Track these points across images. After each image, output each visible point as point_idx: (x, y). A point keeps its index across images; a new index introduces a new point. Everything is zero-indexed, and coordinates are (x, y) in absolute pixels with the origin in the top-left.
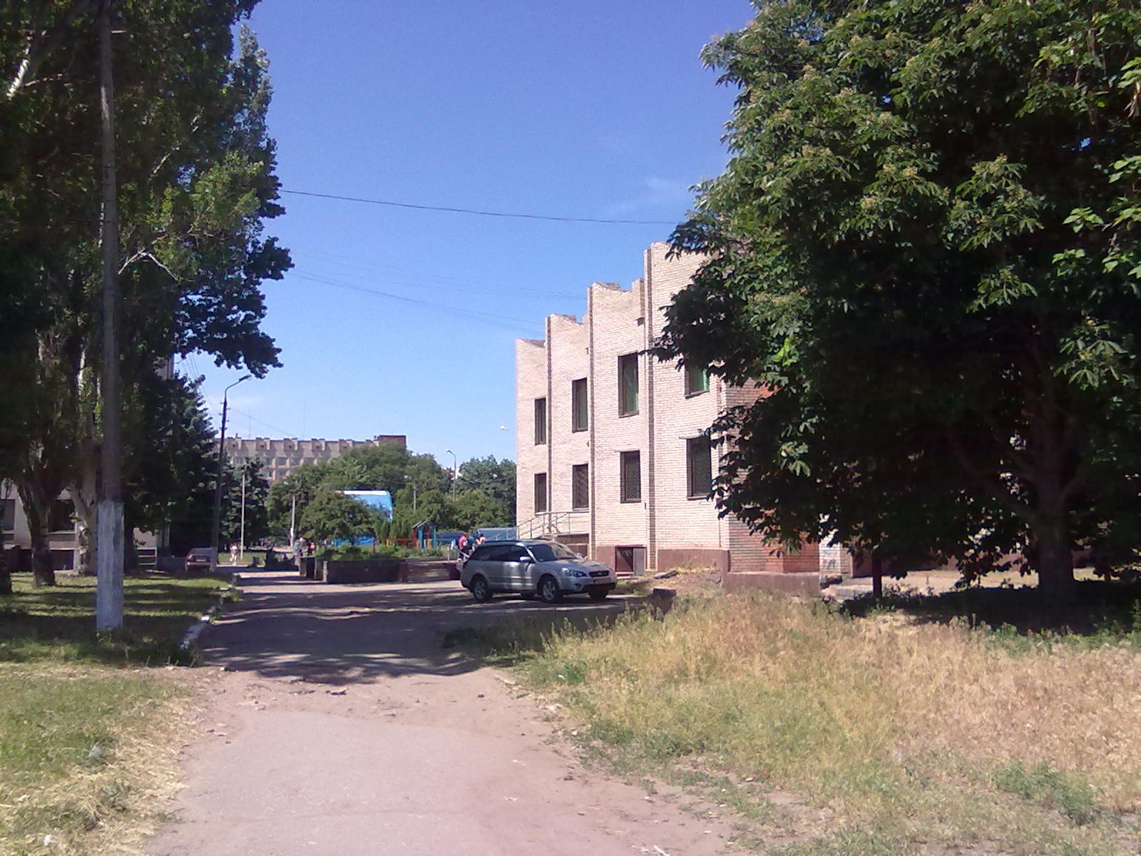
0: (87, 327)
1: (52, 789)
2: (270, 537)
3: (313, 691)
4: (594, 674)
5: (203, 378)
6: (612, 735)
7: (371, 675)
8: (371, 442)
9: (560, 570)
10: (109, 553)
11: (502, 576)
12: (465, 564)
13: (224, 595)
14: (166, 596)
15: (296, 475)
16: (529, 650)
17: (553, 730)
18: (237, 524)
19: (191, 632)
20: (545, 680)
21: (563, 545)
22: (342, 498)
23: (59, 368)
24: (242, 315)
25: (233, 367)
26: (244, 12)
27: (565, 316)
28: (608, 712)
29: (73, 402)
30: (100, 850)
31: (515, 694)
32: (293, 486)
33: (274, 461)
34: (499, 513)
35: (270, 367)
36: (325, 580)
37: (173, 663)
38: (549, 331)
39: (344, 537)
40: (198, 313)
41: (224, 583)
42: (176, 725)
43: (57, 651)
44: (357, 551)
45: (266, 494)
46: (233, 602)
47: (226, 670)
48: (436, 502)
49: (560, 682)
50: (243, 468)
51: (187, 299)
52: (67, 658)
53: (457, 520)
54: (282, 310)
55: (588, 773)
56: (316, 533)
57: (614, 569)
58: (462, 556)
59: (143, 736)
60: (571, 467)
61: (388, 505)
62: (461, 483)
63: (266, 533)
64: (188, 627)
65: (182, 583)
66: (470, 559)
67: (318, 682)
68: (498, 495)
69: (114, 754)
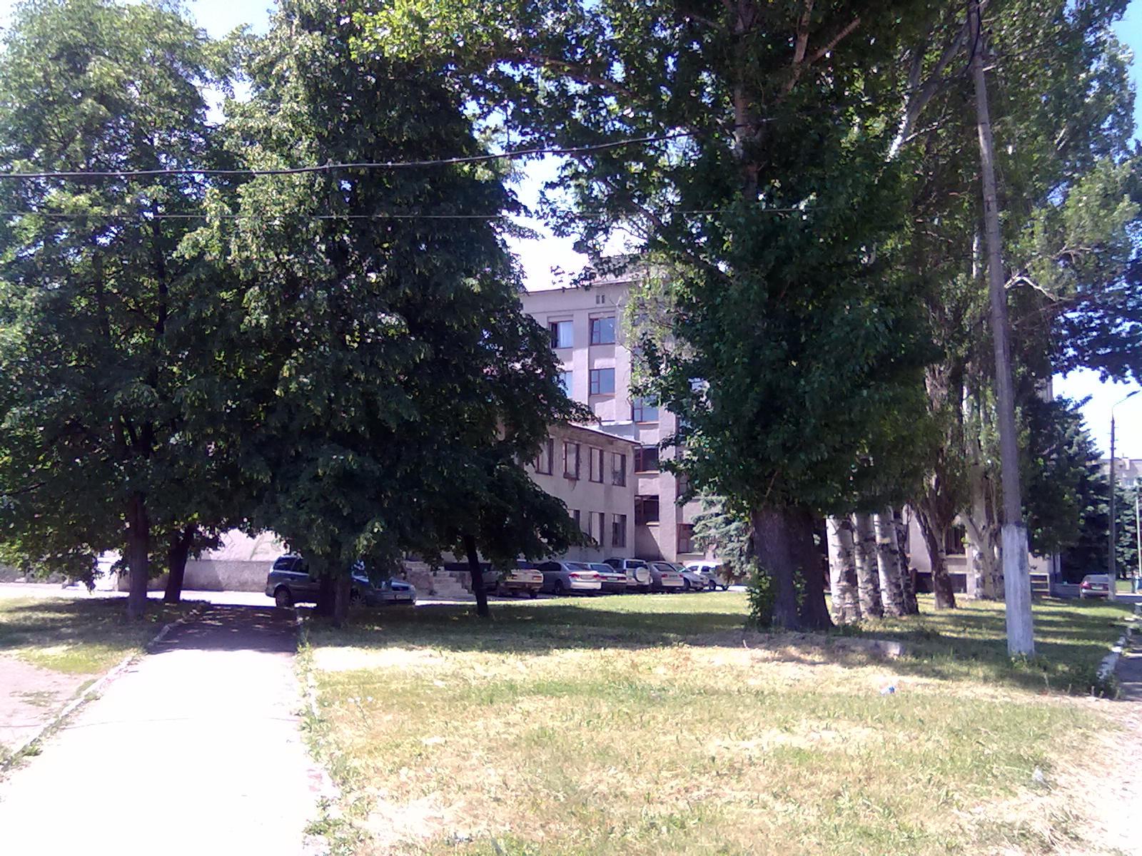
5: (1129, 396)
13: (1132, 626)
14: (1069, 624)
18: (1133, 550)
29: (958, 436)
37: (1097, 695)
50: (1134, 490)
51: (1065, 318)
52: (986, 680)
59: (1080, 765)
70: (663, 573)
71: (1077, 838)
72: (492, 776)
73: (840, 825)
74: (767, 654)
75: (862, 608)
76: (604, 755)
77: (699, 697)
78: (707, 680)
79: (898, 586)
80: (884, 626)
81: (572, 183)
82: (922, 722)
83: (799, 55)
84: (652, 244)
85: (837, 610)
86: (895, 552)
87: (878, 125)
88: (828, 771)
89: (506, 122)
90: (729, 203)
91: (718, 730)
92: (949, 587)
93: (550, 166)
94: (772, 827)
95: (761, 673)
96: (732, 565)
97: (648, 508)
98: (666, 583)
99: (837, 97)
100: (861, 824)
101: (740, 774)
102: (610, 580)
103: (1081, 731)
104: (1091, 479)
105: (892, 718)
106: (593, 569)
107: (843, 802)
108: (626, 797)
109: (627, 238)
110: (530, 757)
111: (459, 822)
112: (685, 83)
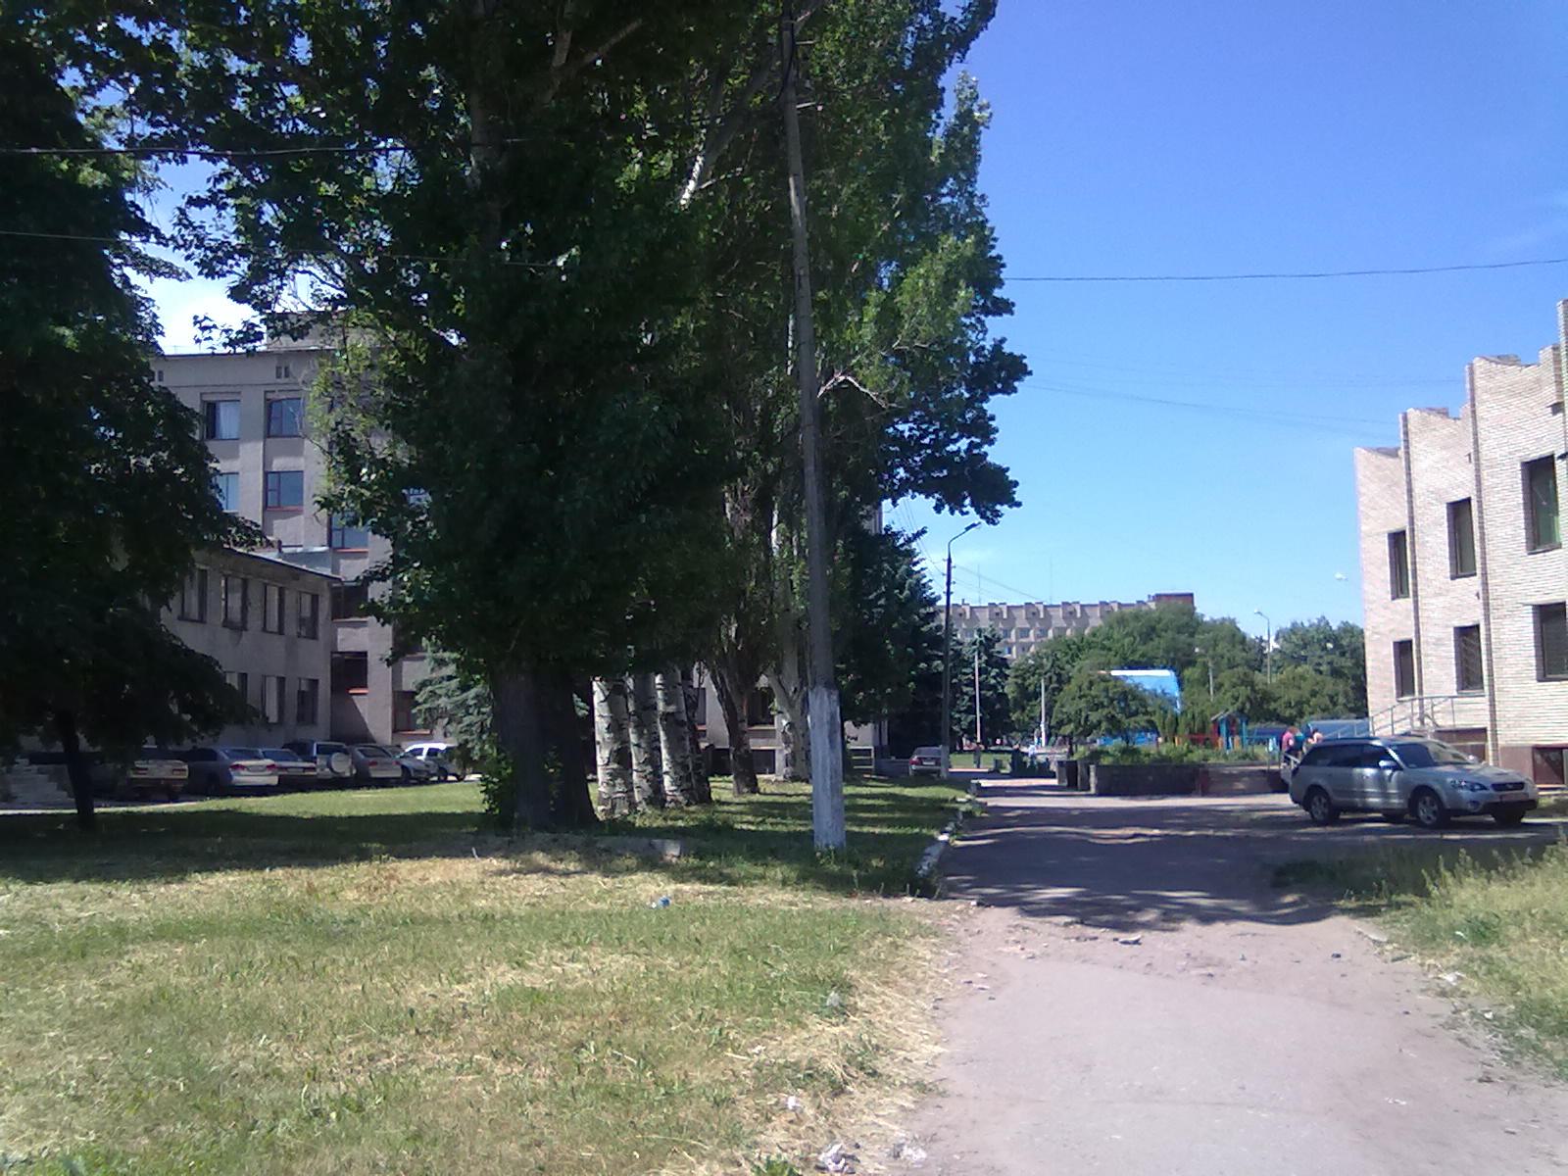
0: (780, 471)
1: (790, 1041)
2: (1013, 734)
3: (1096, 938)
4: (1514, 932)
5: (923, 532)
6: (1550, 1022)
7: (1175, 920)
8: (1145, 604)
9: (1444, 782)
10: (824, 756)
11: (1357, 789)
12: (1295, 772)
13: (963, 808)
14: (891, 809)
15: (1044, 651)
16: (1406, 893)
17: (1453, 1009)
19: (929, 854)
20: (1434, 938)
21: (1445, 744)
22: (1108, 681)
23: (752, 526)
24: (964, 444)
25: (957, 512)
26: (957, 54)
27: (1431, 409)
28: (1540, 988)
29: (765, 573)
30: (852, 1121)
31: (1388, 956)
32: (1042, 666)
33: (1013, 632)
34: (1341, 700)
35: (1003, 509)
36: (1093, 791)
37: (912, 894)
38: (1406, 433)
39: (1114, 733)
40: (909, 446)
41: (962, 793)
42: (924, 973)
43: (773, 873)
44: (1136, 752)
45: (1006, 677)
46: (975, 817)
47: (979, 904)
48: (1243, 683)
49: (1460, 941)
50: (974, 644)
51: (895, 429)
52: (784, 883)
53: (1275, 710)
54: (1018, 432)
55: (1513, 1073)
56: (1077, 728)
57: (1531, 778)
58: (1287, 760)
59: (886, 983)
60: (1452, 630)
61: (1173, 689)
62: (1277, 657)
63: (1009, 728)
64: (925, 848)
65: (908, 792)
66: (1302, 764)
67: (1101, 927)
68: (1336, 673)
69: (856, 1003)
70: (371, 760)
71: (874, 1074)
72: (75, 1063)
73: (579, 1086)
74: (504, 864)
75: (637, 797)
76: (252, 1019)
77: (403, 928)
78: (417, 904)
79: (685, 767)
80: (665, 819)
81: (231, 201)
82: (697, 940)
83: (559, 59)
84: (352, 298)
85: (603, 802)
86: (682, 724)
87: (666, 163)
88: (570, 1016)
89: (126, 103)
90: (460, 250)
91: (423, 973)
92: (750, 767)
93: (196, 173)
94: (486, 1098)
95: (494, 891)
96: (469, 746)
97: (351, 670)
98: (376, 773)
99: (610, 120)
100: (606, 1082)
101: (449, 1030)
102: (292, 772)
103: (889, 940)
104: (924, 629)
105: (660, 939)
106: (266, 756)
107: (587, 1056)
108: (281, 1077)
109: (315, 287)
110: (137, 1030)
111: (12, 1138)
112: (400, 79)
